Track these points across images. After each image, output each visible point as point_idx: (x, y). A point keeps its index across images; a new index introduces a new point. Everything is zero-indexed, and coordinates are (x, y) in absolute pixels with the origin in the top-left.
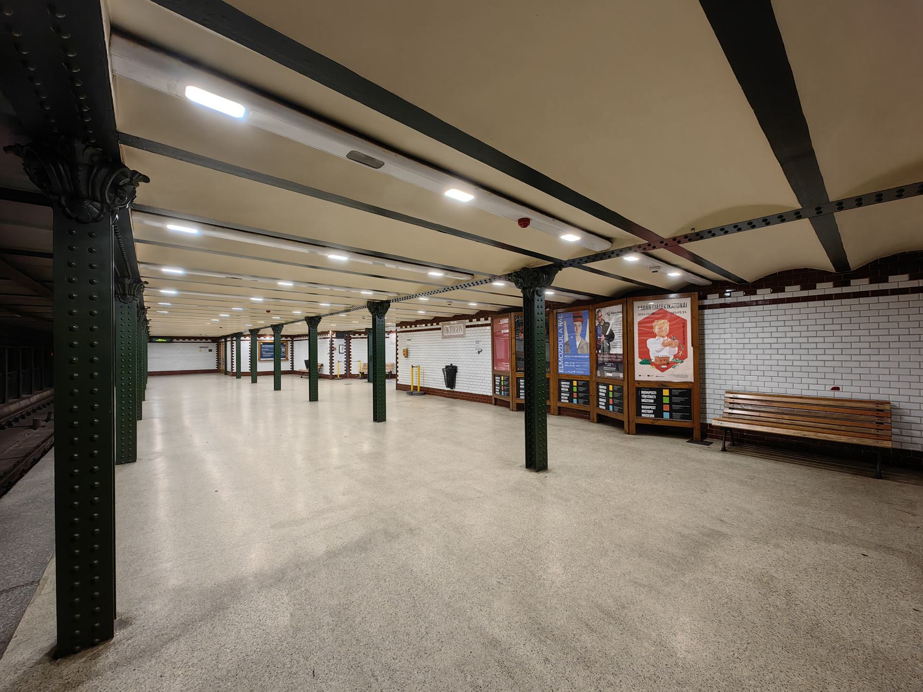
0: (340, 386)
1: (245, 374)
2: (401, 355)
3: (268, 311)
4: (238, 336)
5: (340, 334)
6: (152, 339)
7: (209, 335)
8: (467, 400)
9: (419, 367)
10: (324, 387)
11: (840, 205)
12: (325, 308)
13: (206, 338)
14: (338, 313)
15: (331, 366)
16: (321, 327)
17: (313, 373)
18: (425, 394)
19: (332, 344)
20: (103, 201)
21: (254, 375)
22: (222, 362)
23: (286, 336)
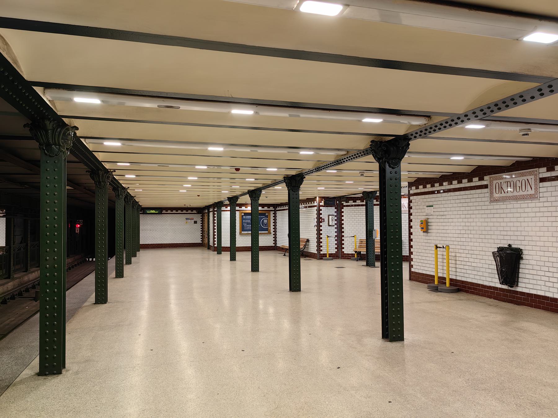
0: (329, 268)
1: (226, 249)
4: (219, 205)
5: (329, 201)
6: (145, 210)
8: (531, 306)
9: (446, 247)
10: (308, 269)
11: (275, 243)
12: (307, 159)
13: (192, 209)
15: (319, 242)
16: (306, 190)
17: (296, 252)
18: (458, 291)
19: (319, 214)
21: (233, 250)
23: (269, 205)
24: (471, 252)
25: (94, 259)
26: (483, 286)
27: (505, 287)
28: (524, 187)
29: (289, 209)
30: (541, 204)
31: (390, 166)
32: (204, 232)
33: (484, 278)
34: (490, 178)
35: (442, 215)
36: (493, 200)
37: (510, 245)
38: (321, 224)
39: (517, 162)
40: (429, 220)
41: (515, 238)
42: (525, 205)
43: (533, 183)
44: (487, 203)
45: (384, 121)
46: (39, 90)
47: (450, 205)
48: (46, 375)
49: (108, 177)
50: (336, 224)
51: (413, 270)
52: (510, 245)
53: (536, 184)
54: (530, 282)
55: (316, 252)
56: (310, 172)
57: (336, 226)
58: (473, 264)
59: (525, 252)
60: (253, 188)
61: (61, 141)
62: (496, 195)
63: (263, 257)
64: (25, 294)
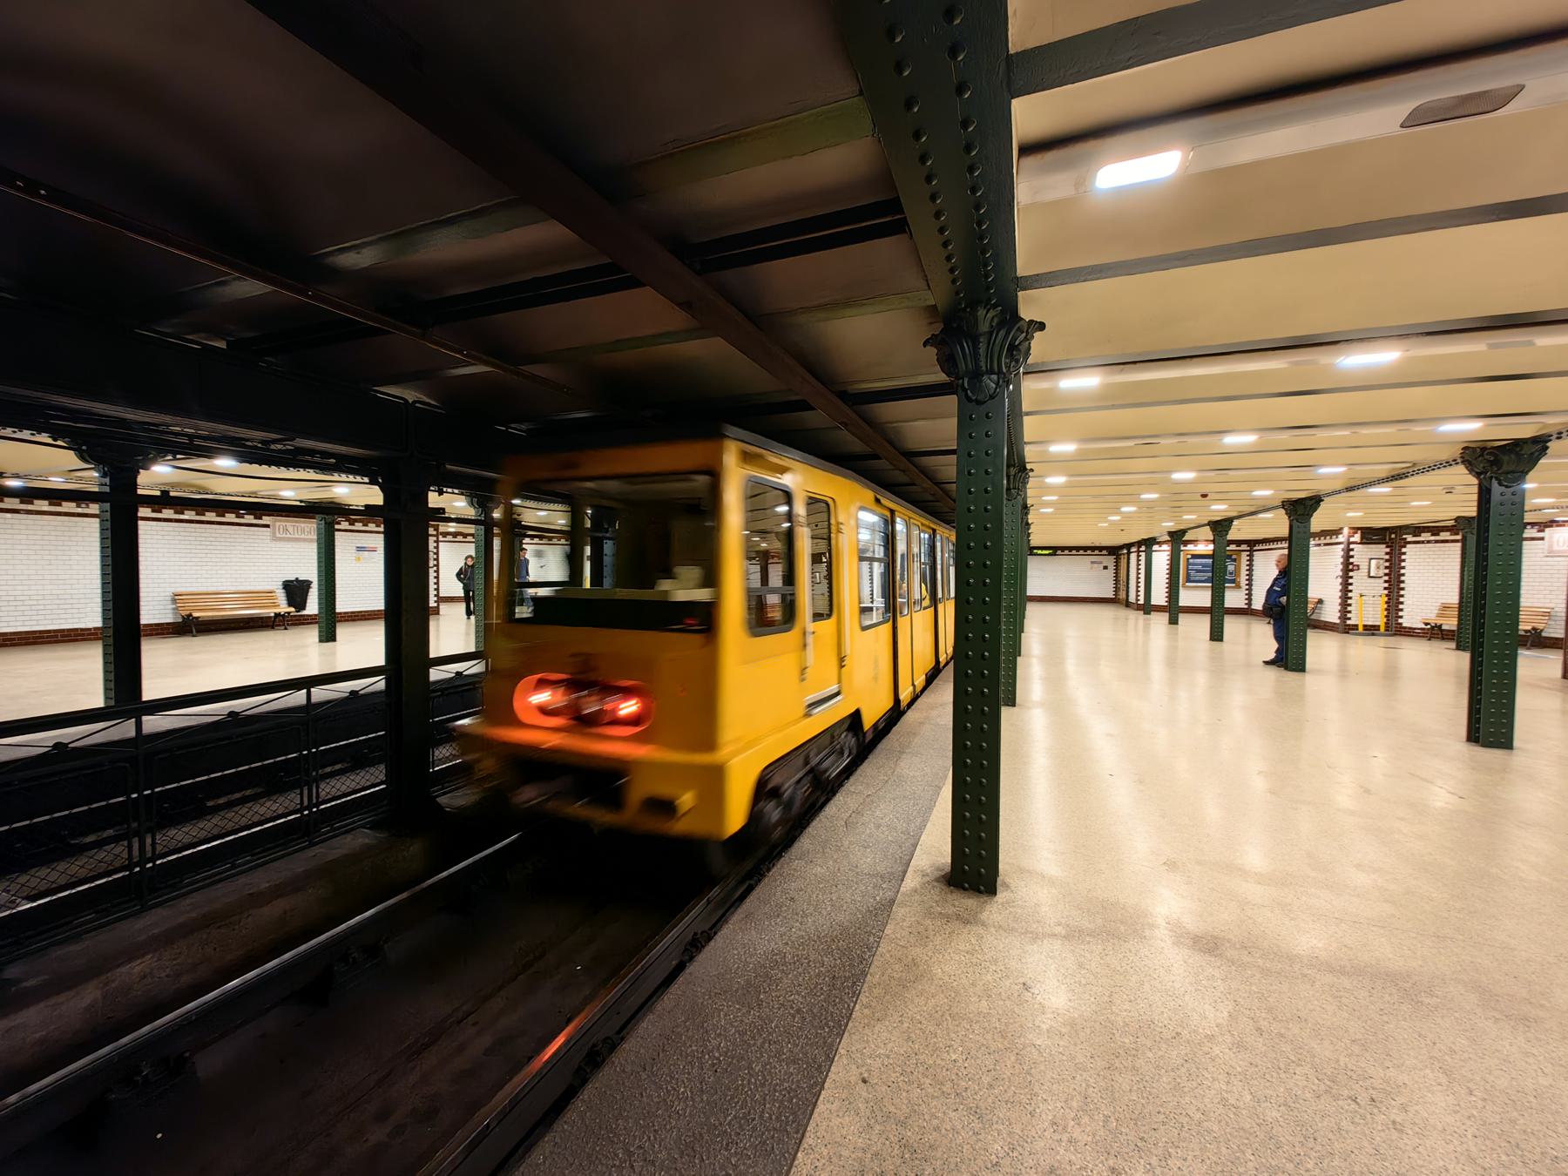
0: (1367, 652)
1: (1159, 609)
3: (1204, 496)
4: (1149, 543)
5: (1371, 535)
7: (1104, 544)
11: (1249, 604)
13: (1101, 548)
19: (1347, 556)
20: (1000, 372)
21: (1174, 611)
22: (1122, 587)
23: (1239, 543)
29: (1290, 548)
32: (1120, 582)
63: (1231, 625)
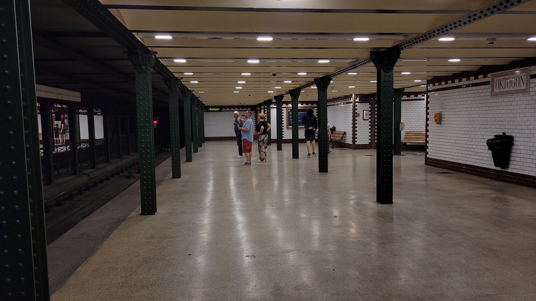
1: (274, 141)
2: (432, 122)
4: (267, 103)
6: (207, 108)
8: (518, 184)
14: (345, 70)
15: (354, 134)
16: (332, 92)
19: (354, 109)
24: (474, 140)
25: (169, 149)
26: (460, 164)
27: (498, 168)
28: (518, 82)
29: (318, 107)
30: (530, 98)
31: (384, 71)
33: (483, 162)
34: (492, 75)
35: (453, 109)
36: (494, 94)
37: (504, 133)
38: (356, 118)
39: (514, 61)
40: (443, 113)
41: (508, 127)
42: (517, 99)
43: (525, 79)
44: (489, 97)
45: (39, 113)
46: (135, 34)
47: (460, 100)
48: (145, 215)
49: (178, 83)
50: (370, 118)
51: (428, 156)
52: (504, 133)
53: (527, 80)
54: (520, 164)
55: (352, 143)
56: (334, 75)
57: (370, 120)
58: (476, 150)
59: (515, 139)
60: (293, 89)
61: (147, 62)
62: (496, 91)
64: (121, 174)
